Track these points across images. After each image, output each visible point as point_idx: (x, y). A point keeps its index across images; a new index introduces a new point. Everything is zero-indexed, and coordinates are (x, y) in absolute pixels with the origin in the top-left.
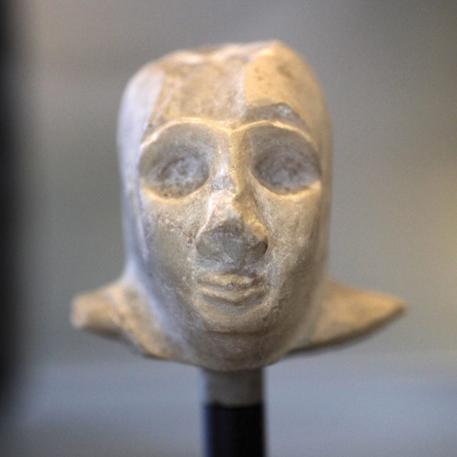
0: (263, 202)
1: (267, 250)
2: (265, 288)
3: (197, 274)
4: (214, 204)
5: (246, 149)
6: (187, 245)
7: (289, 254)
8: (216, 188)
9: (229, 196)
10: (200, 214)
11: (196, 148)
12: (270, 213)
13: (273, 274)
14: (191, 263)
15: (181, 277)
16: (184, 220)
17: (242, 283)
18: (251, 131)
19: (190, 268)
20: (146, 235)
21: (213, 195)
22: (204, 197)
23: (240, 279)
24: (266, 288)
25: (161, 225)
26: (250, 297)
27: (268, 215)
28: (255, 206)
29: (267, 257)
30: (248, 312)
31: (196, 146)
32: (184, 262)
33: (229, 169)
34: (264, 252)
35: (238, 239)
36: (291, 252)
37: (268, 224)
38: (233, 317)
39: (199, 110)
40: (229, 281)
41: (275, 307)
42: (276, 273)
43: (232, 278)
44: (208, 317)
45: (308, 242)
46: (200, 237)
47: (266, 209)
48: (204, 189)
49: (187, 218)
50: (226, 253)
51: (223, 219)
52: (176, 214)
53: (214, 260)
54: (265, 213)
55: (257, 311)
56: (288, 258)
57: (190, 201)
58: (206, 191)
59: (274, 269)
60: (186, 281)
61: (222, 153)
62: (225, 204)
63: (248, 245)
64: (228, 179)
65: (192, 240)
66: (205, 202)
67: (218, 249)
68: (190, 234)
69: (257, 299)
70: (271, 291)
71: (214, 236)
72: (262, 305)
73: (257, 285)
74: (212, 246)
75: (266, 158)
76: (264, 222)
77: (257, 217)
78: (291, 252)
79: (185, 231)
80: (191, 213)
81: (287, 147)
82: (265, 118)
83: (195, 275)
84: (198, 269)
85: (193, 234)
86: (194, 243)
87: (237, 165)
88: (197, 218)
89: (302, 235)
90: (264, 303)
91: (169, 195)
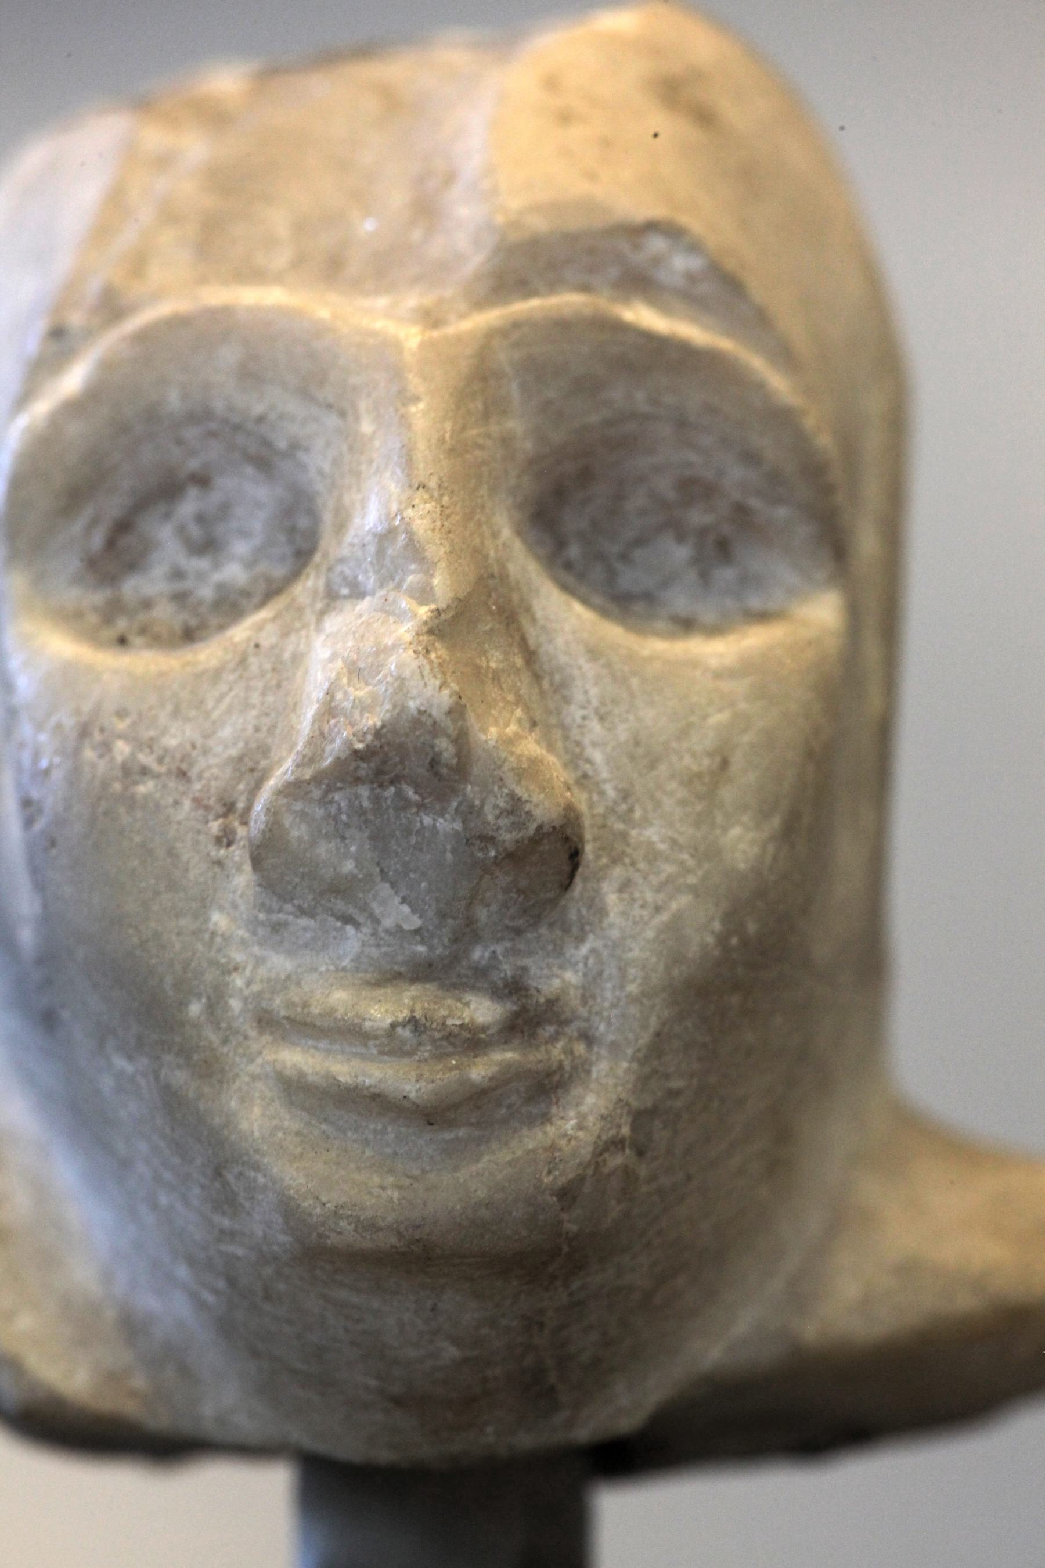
0: (563, 659)
1: (578, 880)
2: (569, 1051)
3: (255, 988)
4: (333, 658)
5: (486, 415)
6: (208, 854)
7: (682, 901)
8: (345, 591)
9: (401, 617)
10: (273, 715)
11: (261, 419)
12: (597, 712)
13: (608, 992)
14: (227, 939)
15: (183, 1004)
16: (198, 744)
17: (458, 1022)
18: (515, 336)
19: (223, 961)
20: (28, 822)
21: (333, 623)
22: (293, 638)
23: (449, 1001)
24: (572, 1052)
25: (93, 766)
26: (494, 1089)
27: (587, 722)
28: (526, 677)
29: (579, 910)
30: (486, 1158)
31: (258, 409)
32: (196, 933)
33: (404, 497)
34: (567, 884)
35: (442, 813)
36: (694, 890)
37: (588, 761)
38: (414, 1178)
39: (281, 259)
40: (402, 1012)
41: (617, 1144)
42: (622, 987)
43: (413, 998)
44: (302, 1180)
45: (771, 849)
46: (268, 809)
47: (579, 697)
48: (294, 600)
49: (214, 732)
50: (387, 885)
51: (372, 720)
52: (163, 718)
53: (331, 919)
54: (575, 713)
55: (528, 1152)
56: (678, 918)
57: (229, 656)
58: (300, 610)
59: (611, 970)
60: (203, 1018)
61: (374, 432)
62: (382, 651)
63: (488, 839)
64: (402, 538)
65: (234, 832)
66: (298, 659)
67: (349, 866)
68: (225, 805)
69: (529, 1099)
70: (594, 1070)
71: (331, 802)
72: (551, 1130)
73: (533, 1035)
74: (324, 850)
75: (586, 476)
76: (567, 752)
77: (534, 724)
78: (694, 890)
79: (200, 791)
80: (229, 711)
81: (682, 424)
82: (585, 288)
83: (246, 993)
84: (260, 961)
85: (240, 805)
86: (242, 843)
87: (440, 479)
88: (257, 729)
89: (745, 818)
90: (562, 1118)
91: (137, 641)
